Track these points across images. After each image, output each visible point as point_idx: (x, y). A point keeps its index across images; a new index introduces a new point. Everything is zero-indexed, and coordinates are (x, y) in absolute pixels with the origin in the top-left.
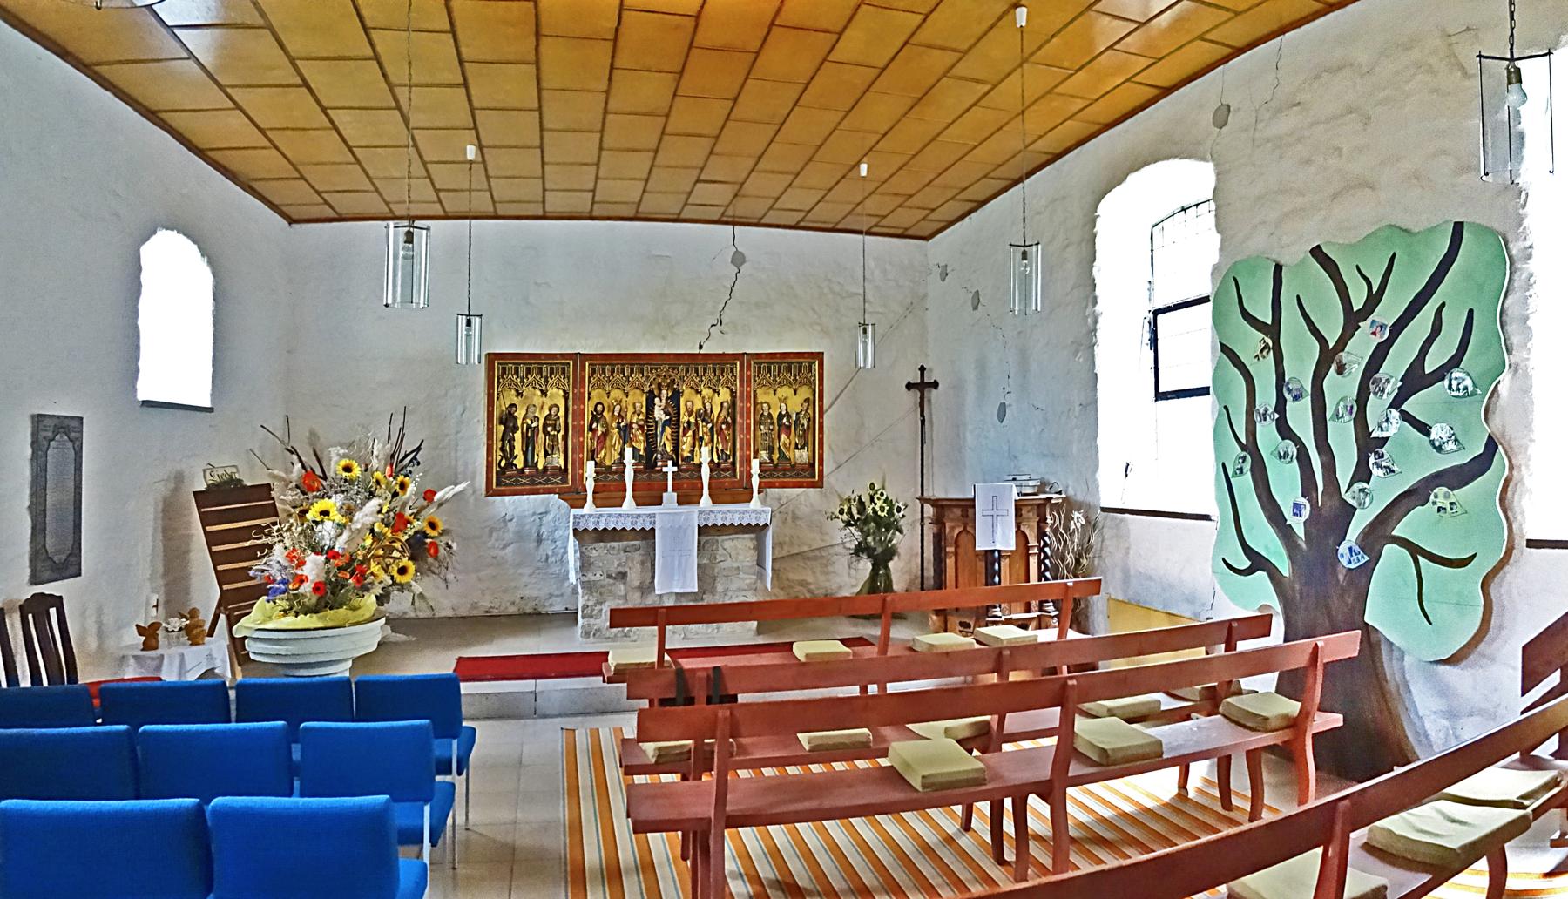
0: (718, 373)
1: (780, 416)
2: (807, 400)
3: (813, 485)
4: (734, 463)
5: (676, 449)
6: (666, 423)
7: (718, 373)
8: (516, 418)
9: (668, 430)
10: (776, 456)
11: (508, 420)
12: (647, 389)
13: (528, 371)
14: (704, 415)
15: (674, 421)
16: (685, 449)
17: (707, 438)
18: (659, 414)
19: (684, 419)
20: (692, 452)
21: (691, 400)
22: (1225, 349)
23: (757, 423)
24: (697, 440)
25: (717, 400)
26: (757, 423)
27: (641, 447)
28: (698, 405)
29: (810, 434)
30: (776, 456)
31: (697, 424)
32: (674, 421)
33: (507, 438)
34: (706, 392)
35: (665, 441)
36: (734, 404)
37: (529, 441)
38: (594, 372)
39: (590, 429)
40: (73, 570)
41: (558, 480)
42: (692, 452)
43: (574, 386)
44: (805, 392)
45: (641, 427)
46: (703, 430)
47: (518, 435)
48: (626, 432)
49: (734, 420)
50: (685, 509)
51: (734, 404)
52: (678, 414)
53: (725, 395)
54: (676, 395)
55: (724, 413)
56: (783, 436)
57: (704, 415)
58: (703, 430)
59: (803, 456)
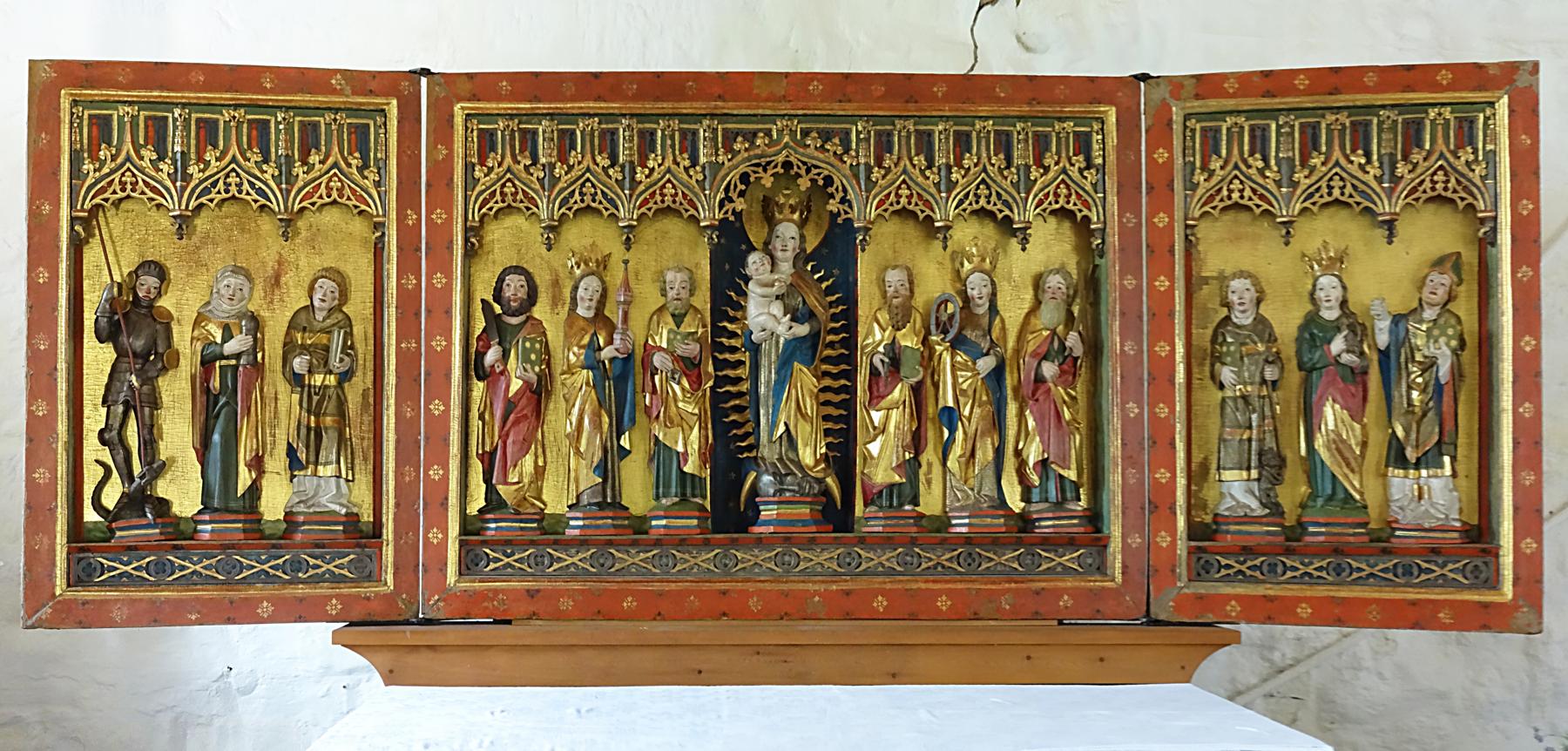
0: (1022, 154)
1: (1314, 331)
2: (1450, 263)
3: (1490, 619)
4: (1094, 518)
5: (842, 455)
6: (803, 349)
7: (1022, 154)
8: (164, 324)
9: (805, 380)
10: (1292, 492)
11: (134, 321)
12: (708, 215)
13: (208, 132)
14: (963, 324)
15: (829, 344)
16: (880, 456)
17: (973, 414)
18: (763, 315)
19: (874, 336)
20: (911, 467)
21: (897, 272)
22: (76, 739)
23: (1206, 359)
24: (928, 420)
25: (1020, 263)
26: (1206, 359)
27: (690, 444)
28: (934, 282)
29: (1462, 408)
30: (1292, 492)
31: (928, 358)
32: (829, 344)
33: (135, 400)
34: (968, 234)
35: (791, 422)
36: (1091, 284)
37: (217, 411)
38: (487, 142)
39: (475, 367)
40: (45, 74)
41: (341, 564)
42: (911, 467)
43: (408, 197)
44: (1432, 233)
45: (689, 367)
46: (957, 380)
47: (176, 389)
48: (620, 385)
49: (1095, 348)
50: (1243, 638)
51: (1091, 284)
52: (851, 327)
53: (1049, 247)
54: (835, 251)
55: (1050, 315)
56: (1331, 414)
57: (963, 324)
58: (957, 380)
59: (1431, 496)
